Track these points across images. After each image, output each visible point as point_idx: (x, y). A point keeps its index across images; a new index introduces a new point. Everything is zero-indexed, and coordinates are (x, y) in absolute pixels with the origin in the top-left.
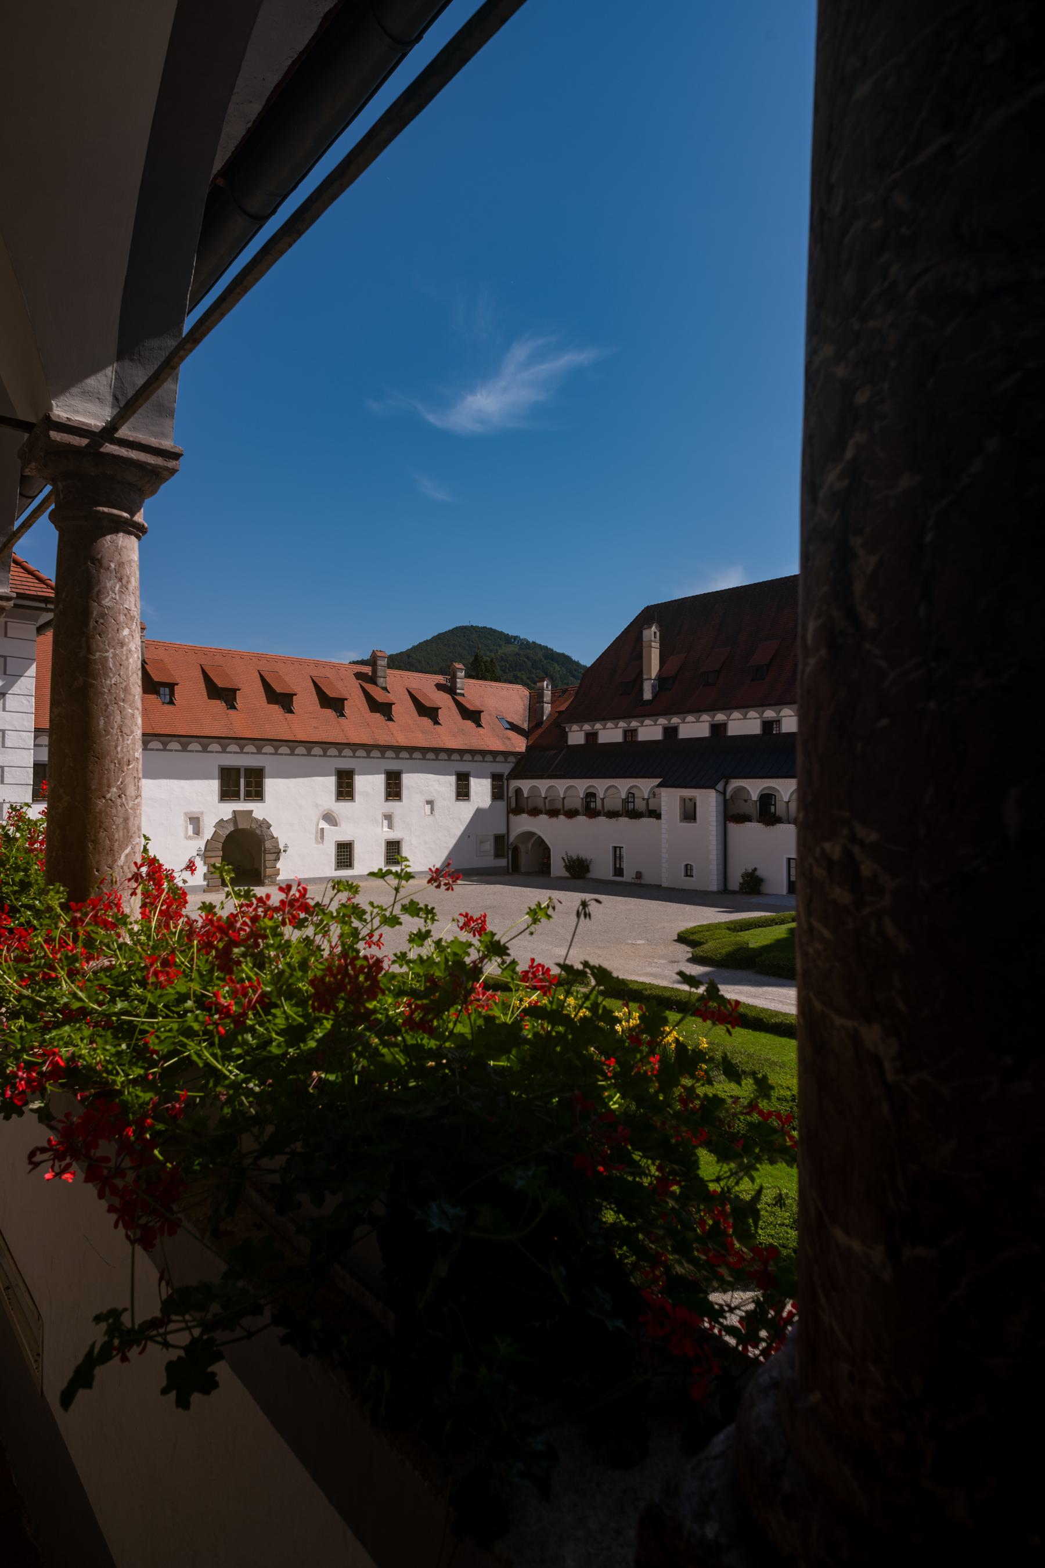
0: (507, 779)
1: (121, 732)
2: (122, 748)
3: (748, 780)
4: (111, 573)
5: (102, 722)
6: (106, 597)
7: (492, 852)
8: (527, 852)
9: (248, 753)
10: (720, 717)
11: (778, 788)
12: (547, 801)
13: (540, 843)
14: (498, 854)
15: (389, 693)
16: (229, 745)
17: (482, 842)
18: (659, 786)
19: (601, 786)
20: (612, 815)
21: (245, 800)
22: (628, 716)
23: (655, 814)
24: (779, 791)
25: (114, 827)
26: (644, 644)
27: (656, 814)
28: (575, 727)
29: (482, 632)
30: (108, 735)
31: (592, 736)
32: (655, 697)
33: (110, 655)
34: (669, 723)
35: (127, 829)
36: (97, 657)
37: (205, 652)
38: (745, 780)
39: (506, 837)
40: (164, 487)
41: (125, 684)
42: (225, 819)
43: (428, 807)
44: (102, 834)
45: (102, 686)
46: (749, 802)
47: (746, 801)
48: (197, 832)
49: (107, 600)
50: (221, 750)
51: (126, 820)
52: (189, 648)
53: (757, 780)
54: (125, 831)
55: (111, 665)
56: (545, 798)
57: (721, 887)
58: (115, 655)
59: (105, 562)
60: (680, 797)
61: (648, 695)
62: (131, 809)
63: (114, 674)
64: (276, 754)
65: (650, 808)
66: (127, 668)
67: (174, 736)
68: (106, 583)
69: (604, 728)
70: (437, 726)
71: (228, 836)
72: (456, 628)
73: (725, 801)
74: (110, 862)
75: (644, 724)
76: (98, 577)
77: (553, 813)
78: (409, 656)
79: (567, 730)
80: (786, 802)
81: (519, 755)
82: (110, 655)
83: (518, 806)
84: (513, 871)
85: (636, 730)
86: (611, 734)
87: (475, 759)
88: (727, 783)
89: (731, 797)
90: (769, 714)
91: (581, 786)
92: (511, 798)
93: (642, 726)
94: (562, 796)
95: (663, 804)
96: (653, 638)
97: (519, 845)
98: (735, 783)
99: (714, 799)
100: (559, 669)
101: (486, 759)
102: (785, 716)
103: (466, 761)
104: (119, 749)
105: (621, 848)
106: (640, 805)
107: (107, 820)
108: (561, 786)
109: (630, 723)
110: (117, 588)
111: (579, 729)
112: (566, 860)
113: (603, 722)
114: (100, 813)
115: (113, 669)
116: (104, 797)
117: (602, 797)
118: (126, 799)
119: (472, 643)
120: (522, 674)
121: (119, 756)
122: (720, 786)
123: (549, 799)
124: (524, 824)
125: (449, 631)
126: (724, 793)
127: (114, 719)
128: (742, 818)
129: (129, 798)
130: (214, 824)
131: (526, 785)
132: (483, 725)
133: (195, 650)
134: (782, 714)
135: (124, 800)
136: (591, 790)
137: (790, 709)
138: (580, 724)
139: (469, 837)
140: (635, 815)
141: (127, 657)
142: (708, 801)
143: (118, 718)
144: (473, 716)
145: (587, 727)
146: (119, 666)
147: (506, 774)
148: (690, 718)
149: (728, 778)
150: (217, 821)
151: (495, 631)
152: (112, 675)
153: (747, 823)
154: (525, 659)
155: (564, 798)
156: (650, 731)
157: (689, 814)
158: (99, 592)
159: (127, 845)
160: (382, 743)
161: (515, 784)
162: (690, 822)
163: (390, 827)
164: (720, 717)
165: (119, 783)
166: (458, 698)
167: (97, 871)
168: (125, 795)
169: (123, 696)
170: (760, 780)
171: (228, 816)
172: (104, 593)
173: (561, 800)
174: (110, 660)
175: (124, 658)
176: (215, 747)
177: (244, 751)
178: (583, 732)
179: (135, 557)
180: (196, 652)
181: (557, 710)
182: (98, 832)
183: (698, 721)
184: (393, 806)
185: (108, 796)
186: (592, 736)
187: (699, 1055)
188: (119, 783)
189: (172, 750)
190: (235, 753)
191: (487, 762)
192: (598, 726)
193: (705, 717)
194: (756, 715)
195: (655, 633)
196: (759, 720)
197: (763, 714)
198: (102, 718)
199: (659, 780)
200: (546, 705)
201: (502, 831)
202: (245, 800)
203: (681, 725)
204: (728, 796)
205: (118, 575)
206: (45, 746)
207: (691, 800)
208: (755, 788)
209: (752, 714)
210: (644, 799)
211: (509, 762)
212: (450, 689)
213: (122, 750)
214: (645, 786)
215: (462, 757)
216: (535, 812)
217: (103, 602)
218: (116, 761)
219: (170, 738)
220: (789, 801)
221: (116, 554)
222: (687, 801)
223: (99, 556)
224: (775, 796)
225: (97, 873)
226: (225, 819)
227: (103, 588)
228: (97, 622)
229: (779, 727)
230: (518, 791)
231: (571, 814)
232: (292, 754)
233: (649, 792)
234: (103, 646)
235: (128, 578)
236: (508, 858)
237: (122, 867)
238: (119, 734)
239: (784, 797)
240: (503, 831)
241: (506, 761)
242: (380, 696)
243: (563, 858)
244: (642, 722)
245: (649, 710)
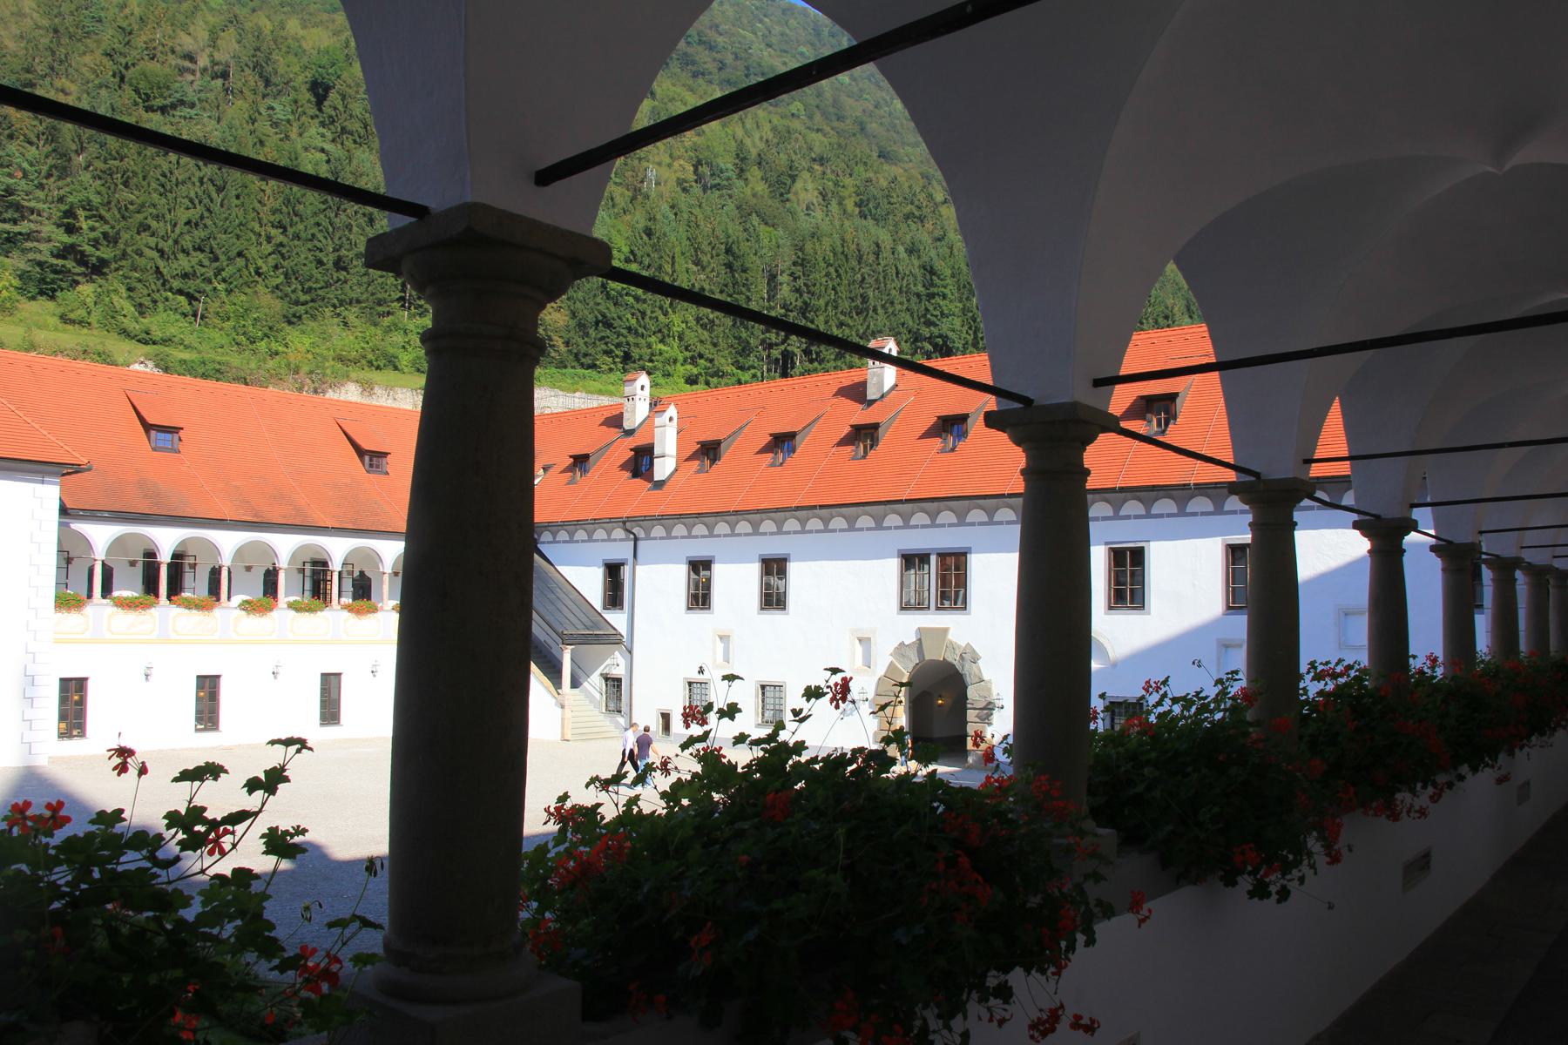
16: (998, 509)
21: (938, 609)
42: (906, 643)
43: (720, 646)
50: (902, 524)
64: (991, 522)
67: (1002, 496)
87: (693, 533)
101: (694, 532)
112: (297, 839)
171: (911, 638)
187: (181, 57)
206: (1096, 519)
215: (1117, 509)
226: (906, 643)
232: (851, 528)
243: (304, 831)
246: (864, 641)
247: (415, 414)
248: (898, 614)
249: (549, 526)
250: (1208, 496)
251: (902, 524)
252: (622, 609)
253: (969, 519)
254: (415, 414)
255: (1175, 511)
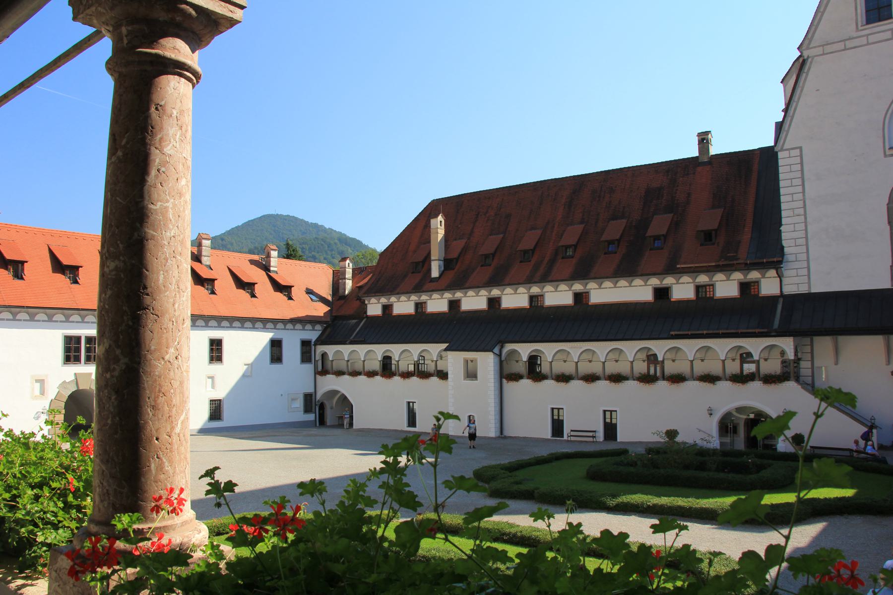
0: (315, 345)
1: (178, 288)
2: (179, 305)
3: (520, 344)
4: (173, 121)
5: (161, 277)
6: (168, 145)
7: (302, 408)
8: (332, 408)
9: (88, 322)
10: (495, 292)
11: (545, 352)
12: (349, 363)
13: (344, 399)
14: (308, 409)
15: (212, 270)
16: (86, 316)
17: (293, 400)
18: (446, 350)
19: (395, 350)
20: (406, 375)
21: (85, 363)
22: (418, 289)
23: (443, 375)
24: (544, 353)
25: (172, 391)
26: (432, 231)
27: (443, 375)
28: (373, 300)
29: (286, 220)
30: (166, 291)
31: (387, 308)
32: (441, 275)
33: (170, 205)
34: (661, 284)
35: (182, 393)
36: (158, 207)
37: (52, 234)
38: (517, 344)
39: (314, 395)
40: (218, 40)
41: (181, 236)
44: (161, 400)
45: (162, 239)
46: (519, 362)
47: (517, 361)
48: (43, 392)
49: (169, 148)
50: (64, 320)
51: (181, 383)
52: (38, 230)
53: (526, 344)
54: (181, 395)
55: (171, 216)
56: (348, 361)
57: (498, 434)
58: (175, 205)
59: (168, 109)
60: (464, 359)
61: (435, 273)
62: (185, 371)
63: (174, 226)
65: (438, 369)
66: (184, 220)
67: (23, 307)
68: (168, 130)
69: (398, 301)
70: (253, 299)
71: (69, 397)
72: (264, 216)
73: (501, 362)
74: (169, 430)
75: (432, 298)
76: (162, 123)
77: (355, 374)
78: (222, 240)
79: (366, 302)
80: (549, 362)
81: (325, 324)
82: (170, 205)
83: (323, 371)
84: (320, 424)
85: (425, 303)
86: (404, 306)
88: (502, 347)
89: (506, 358)
90: (535, 290)
91: (379, 350)
92: (317, 361)
93: (431, 299)
94: (363, 359)
95: (449, 365)
96: (439, 226)
97: (325, 402)
98: (509, 347)
99: (492, 361)
100: (351, 251)
102: (548, 292)
103: (307, 330)
104: (176, 306)
105: (413, 403)
106: (431, 368)
107: (166, 384)
108: (362, 350)
109: (421, 296)
110: (178, 136)
111: (377, 302)
113: (398, 296)
114: (160, 377)
115: (173, 220)
116: (163, 359)
117: (397, 359)
118: (182, 361)
119: (277, 229)
120: (320, 255)
121: (177, 314)
122: (496, 350)
123: (350, 361)
124: (329, 383)
125: (257, 218)
126: (500, 355)
127: (172, 274)
128: (515, 377)
129: (184, 359)
130: (58, 385)
131: (330, 350)
132: (293, 298)
133: (43, 233)
134: (545, 289)
135: (180, 361)
136: (388, 354)
137: (626, 281)
138: (378, 297)
139: (282, 395)
140: (424, 375)
141: (184, 208)
142: (486, 362)
143: (176, 273)
144: (284, 289)
145: (384, 300)
146: (177, 217)
147: (313, 341)
148: (471, 293)
149: (502, 343)
150: (61, 382)
151: (296, 219)
152: (171, 227)
153: (786, 382)
154: (323, 243)
155: (364, 361)
156: (437, 304)
157: (471, 375)
158: (161, 139)
159: (183, 411)
160: (206, 313)
161: (321, 349)
162: (473, 380)
163: (213, 387)
164: (535, 290)
165: (176, 343)
166: (271, 274)
167: (157, 439)
168: (181, 357)
169: (180, 249)
170: (529, 344)
172: (166, 141)
173: (362, 363)
174: (170, 210)
175: (182, 209)
176: (59, 317)
177: (85, 320)
178: (571, 292)
179: (189, 104)
180: (44, 234)
181: (357, 286)
182: (158, 397)
183: (477, 295)
184: (216, 367)
185: (167, 357)
186: (387, 308)
188: (176, 343)
189: (20, 320)
190: (77, 322)
191: (297, 330)
192: (393, 299)
193: (483, 292)
194: (690, 280)
195: (441, 222)
196: (692, 284)
197: (530, 290)
198: (162, 272)
199: (446, 345)
200: (347, 281)
201: (311, 390)
202: (85, 363)
203: (428, 301)
204: (503, 358)
205: (179, 122)
207: (472, 361)
208: (525, 350)
209: (522, 290)
210: (432, 361)
211: (316, 330)
212: (266, 268)
213: (178, 307)
214: (434, 349)
216: (339, 373)
217: (165, 150)
218: (174, 320)
219: (18, 310)
220: (552, 361)
221: (178, 101)
222: (469, 362)
223: (162, 103)
224: (540, 357)
225: (156, 442)
226: (67, 381)
227: (166, 135)
228: (158, 170)
229: (713, 291)
230: (324, 355)
231: (371, 374)
233: (437, 355)
234: (164, 195)
235: (187, 126)
236: (315, 413)
237: (179, 434)
238: (177, 289)
239: (548, 359)
240: (312, 390)
241: (313, 329)
242: (205, 274)
244: (431, 296)
245: (437, 286)
246: (42, 382)
247: (98, 237)
248: (62, 366)
249: (888, 337)
250: (216, 320)
251: (64, 320)
252: (80, 363)
253: (71, 319)
254: (98, 237)
255: (217, 325)
